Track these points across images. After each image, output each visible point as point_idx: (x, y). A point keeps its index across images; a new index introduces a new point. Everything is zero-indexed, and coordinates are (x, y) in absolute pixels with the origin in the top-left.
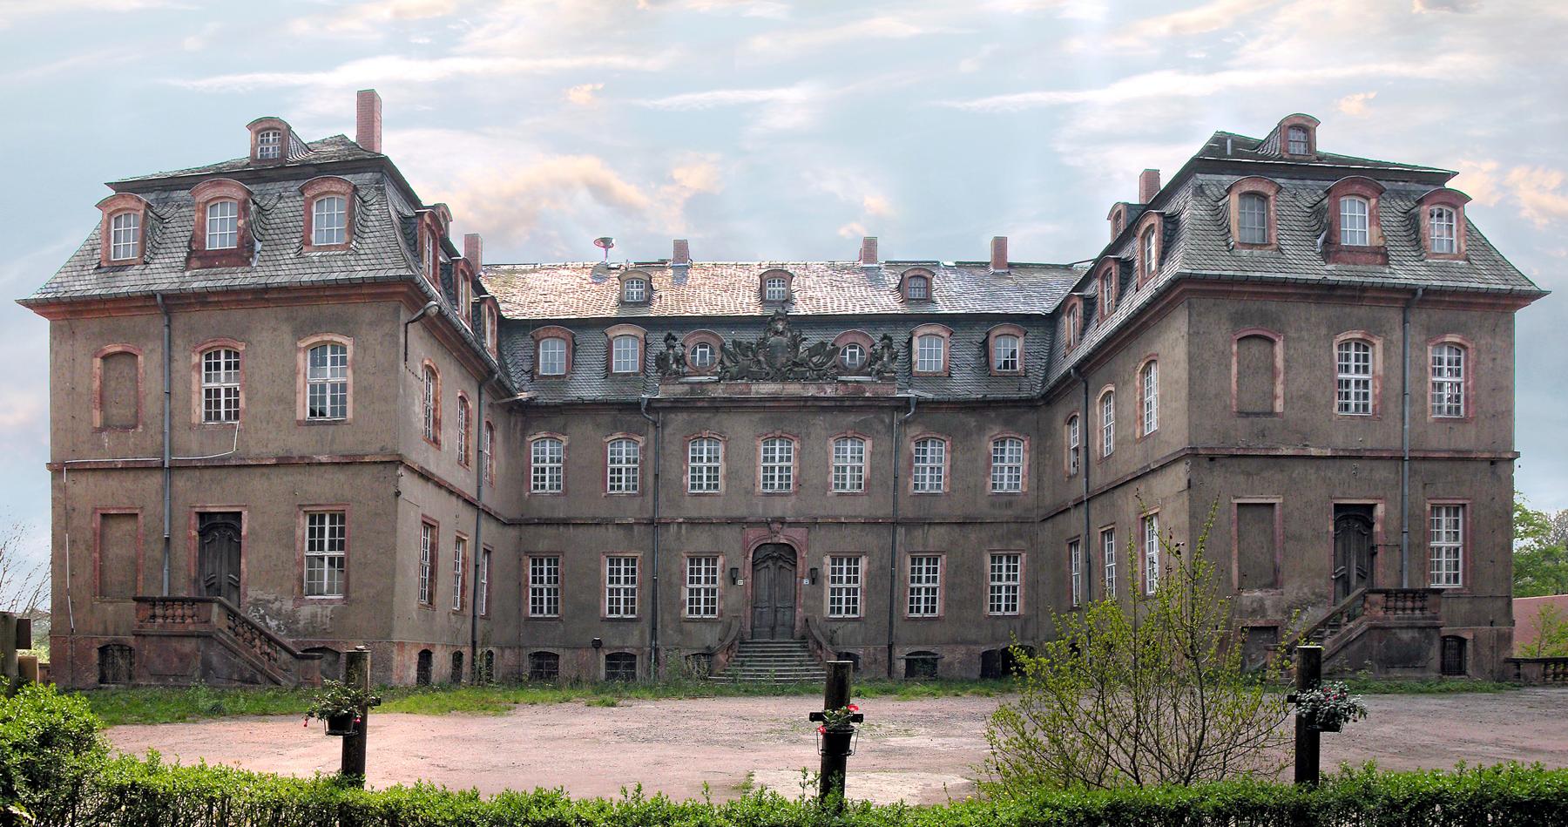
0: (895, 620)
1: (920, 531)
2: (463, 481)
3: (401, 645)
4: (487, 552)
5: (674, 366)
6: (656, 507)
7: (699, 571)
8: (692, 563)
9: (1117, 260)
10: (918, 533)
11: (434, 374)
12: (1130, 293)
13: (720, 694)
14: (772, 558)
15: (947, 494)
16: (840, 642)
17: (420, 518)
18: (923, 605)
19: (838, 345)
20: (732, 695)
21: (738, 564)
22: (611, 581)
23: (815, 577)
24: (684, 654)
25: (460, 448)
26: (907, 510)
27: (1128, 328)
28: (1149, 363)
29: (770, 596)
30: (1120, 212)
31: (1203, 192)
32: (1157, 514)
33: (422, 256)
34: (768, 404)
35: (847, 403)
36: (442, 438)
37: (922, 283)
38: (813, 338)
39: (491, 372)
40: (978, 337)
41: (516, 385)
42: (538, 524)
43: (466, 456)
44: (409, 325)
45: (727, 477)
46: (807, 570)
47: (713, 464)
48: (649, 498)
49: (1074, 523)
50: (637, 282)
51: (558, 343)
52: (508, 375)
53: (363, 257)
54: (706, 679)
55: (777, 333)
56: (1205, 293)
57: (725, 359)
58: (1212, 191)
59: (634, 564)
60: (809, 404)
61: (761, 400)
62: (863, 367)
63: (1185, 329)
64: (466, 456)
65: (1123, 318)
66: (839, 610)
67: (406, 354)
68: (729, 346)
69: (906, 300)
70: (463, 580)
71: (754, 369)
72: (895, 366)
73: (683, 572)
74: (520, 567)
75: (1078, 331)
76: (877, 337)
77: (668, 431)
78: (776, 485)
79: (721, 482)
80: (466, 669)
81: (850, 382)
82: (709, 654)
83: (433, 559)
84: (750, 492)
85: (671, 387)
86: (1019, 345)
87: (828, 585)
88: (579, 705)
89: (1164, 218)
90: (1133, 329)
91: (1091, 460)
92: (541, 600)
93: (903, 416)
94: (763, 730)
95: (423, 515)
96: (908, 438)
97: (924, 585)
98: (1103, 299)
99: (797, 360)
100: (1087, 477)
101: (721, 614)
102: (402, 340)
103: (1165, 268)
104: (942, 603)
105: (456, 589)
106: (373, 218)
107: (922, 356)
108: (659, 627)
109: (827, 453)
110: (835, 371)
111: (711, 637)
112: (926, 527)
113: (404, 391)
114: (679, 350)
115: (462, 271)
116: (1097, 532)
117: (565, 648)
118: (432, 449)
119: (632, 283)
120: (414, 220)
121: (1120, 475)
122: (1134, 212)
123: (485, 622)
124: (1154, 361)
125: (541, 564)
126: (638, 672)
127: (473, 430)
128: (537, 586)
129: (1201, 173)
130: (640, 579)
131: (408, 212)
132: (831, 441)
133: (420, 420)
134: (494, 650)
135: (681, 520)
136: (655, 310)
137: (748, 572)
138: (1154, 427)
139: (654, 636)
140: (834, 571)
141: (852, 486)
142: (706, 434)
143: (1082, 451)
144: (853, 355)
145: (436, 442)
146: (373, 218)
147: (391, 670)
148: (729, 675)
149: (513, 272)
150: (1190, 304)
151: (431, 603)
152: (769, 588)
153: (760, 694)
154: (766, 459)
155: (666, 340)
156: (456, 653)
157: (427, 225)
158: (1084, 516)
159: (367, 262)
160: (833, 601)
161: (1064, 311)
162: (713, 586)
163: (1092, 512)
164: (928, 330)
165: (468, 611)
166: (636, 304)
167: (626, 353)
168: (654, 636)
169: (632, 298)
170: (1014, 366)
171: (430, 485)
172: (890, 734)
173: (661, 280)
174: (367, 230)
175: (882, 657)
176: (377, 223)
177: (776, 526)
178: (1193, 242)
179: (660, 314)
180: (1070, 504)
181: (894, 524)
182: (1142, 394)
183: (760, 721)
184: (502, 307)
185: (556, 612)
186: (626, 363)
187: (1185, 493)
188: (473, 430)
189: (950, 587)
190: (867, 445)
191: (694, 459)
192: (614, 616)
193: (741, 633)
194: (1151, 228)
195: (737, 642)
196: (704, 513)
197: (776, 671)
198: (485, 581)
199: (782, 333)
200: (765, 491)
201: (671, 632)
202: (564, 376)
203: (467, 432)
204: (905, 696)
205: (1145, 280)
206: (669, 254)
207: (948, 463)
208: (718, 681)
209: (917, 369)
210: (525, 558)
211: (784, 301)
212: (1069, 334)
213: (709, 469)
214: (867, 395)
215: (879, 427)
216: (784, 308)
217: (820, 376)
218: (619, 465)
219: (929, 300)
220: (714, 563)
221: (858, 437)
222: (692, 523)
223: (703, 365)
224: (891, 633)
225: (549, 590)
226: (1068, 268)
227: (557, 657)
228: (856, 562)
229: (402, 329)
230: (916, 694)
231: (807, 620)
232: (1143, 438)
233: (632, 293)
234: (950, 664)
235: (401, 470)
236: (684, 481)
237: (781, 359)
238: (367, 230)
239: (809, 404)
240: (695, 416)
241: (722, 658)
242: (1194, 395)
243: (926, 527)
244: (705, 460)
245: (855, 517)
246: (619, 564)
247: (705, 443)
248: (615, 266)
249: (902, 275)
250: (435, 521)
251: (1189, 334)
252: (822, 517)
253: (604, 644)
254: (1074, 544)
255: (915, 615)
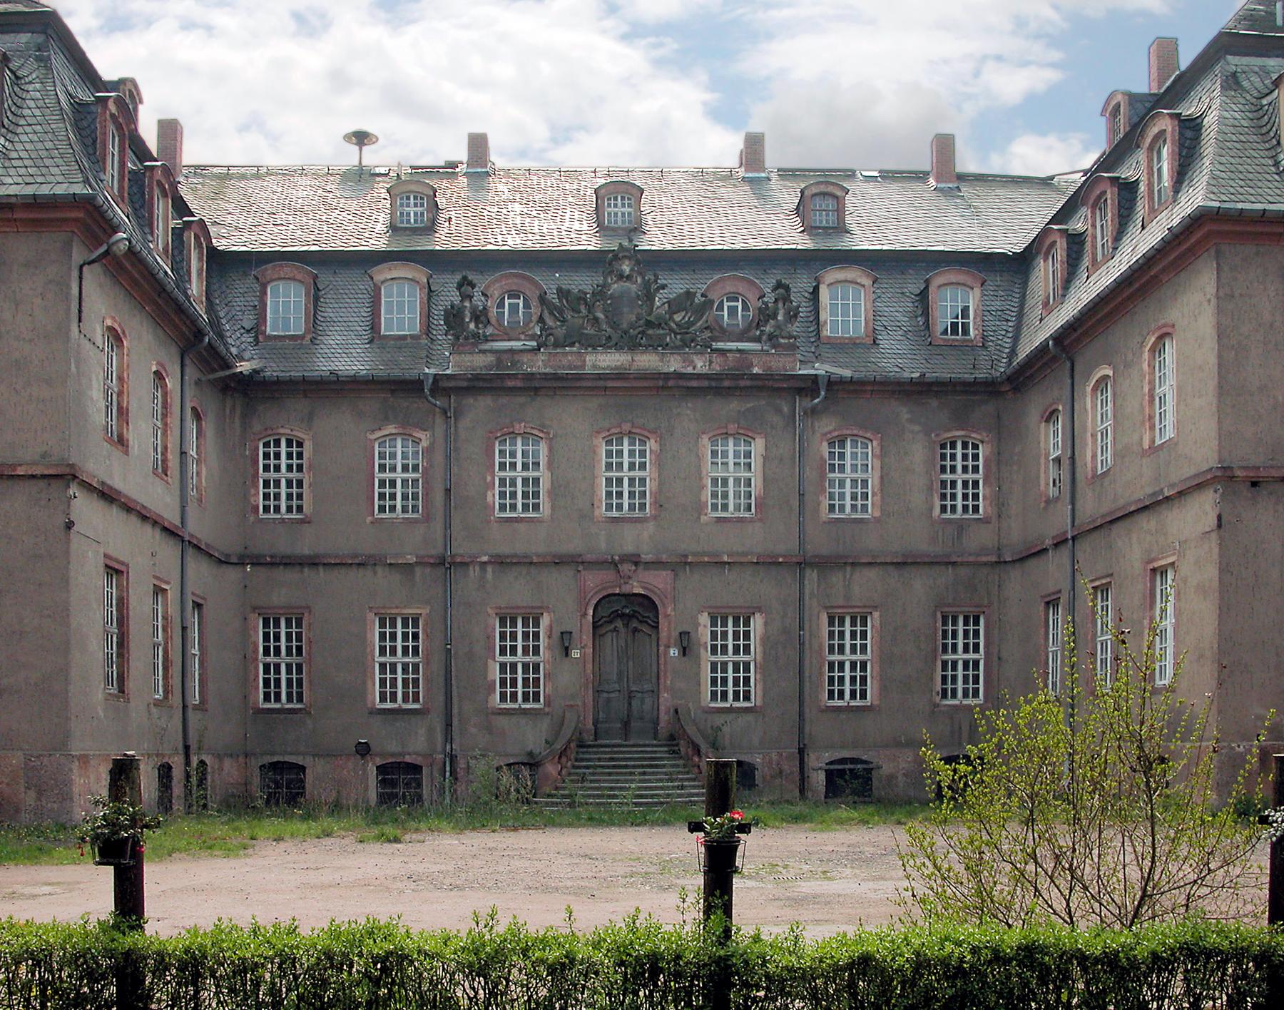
0: (807, 710)
1: (840, 575)
2: (161, 500)
3: (84, 759)
4: (198, 606)
5: (472, 326)
6: (448, 539)
7: (514, 637)
8: (503, 623)
9: (1114, 180)
10: (837, 579)
11: (119, 340)
12: (1134, 229)
13: (550, 823)
14: (622, 616)
15: (877, 520)
16: (727, 743)
17: (101, 561)
18: (847, 688)
19: (710, 296)
20: (570, 825)
21: (572, 625)
22: (382, 651)
23: (686, 644)
24: (495, 763)
25: (156, 450)
26: (820, 544)
27: (1131, 284)
28: (1161, 338)
29: (620, 674)
30: (1118, 105)
31: (1238, 83)
32: (1173, 564)
33: (104, 163)
34: (610, 384)
35: (726, 383)
36: (131, 436)
37: (831, 204)
38: (676, 285)
39: (199, 334)
40: (915, 287)
41: (234, 351)
42: (272, 564)
43: (164, 461)
44: (85, 269)
45: (553, 493)
46: (675, 634)
47: (531, 474)
48: (438, 527)
49: (1053, 570)
50: (415, 198)
51: (293, 286)
52: (221, 336)
53: (15, 163)
54: (528, 802)
55: (621, 277)
56: (1242, 237)
57: (546, 316)
58: (1252, 83)
59: (416, 625)
60: (671, 383)
61: (600, 377)
62: (748, 329)
63: (1211, 289)
64: (164, 461)
65: (1124, 268)
66: (724, 695)
67: (80, 311)
68: (552, 296)
69: (809, 229)
70: (166, 652)
71: (589, 330)
72: (795, 328)
73: (490, 638)
74: (245, 632)
75: (1059, 283)
76: (767, 284)
77: (465, 422)
78: (626, 506)
79: (544, 500)
80: (178, 789)
81: (730, 351)
82: (533, 764)
83: (122, 622)
84: (586, 516)
85: (467, 358)
86: (973, 300)
87: (707, 658)
88: (346, 841)
89: (1181, 121)
90: (1137, 285)
91: (1078, 475)
92: (278, 681)
93: (808, 403)
94: (622, 873)
95: (106, 556)
96: (818, 435)
97: (848, 657)
98: (1095, 237)
99: (651, 318)
100: (1073, 503)
101: (548, 703)
102: (75, 291)
103: (1183, 198)
104: (876, 685)
105: (155, 666)
106: (32, 104)
107: (834, 313)
108: (455, 722)
109: (699, 458)
110: (708, 334)
111: (533, 738)
112: (849, 569)
113: (77, 367)
114: (478, 300)
115: (159, 183)
116: (1085, 584)
117: (314, 756)
118: (117, 453)
119: (408, 198)
120: (93, 108)
121: (1121, 502)
122: (1139, 105)
123: (199, 715)
124: (1168, 334)
125: (277, 625)
126: (425, 792)
127: (174, 421)
128: (271, 659)
129: (1235, 54)
130: (426, 649)
131: (84, 95)
132: (705, 440)
133: (99, 411)
134: (208, 761)
135: (485, 559)
136: (443, 241)
137: (587, 638)
138: (1170, 433)
139: (448, 737)
140: (714, 636)
141: (738, 508)
142: (520, 427)
143: (1066, 463)
144: (733, 311)
145: (122, 442)
146: (32, 104)
147: (71, 799)
148: (564, 796)
149: (227, 176)
150: (1218, 252)
151: (122, 691)
152: (619, 663)
153: (611, 823)
154: (609, 467)
155: (459, 287)
156: (162, 766)
157: (112, 115)
158: (1066, 561)
159: (22, 171)
160: (714, 681)
161: (1038, 253)
162: (535, 659)
163: (1080, 555)
164: (840, 275)
165: (176, 699)
166: (415, 231)
167: (401, 305)
168: (448, 737)
169: (409, 221)
170: (966, 331)
171: (115, 510)
172: (801, 876)
173: (449, 194)
174: (22, 122)
175: (791, 767)
176: (37, 112)
177: (626, 568)
178: (1223, 160)
179: (451, 247)
180: (1048, 542)
181: (802, 565)
182: (1152, 383)
183: (614, 860)
184: (213, 230)
185: (300, 700)
186: (401, 321)
187: (1214, 536)
188: (174, 421)
189: (886, 659)
190: (758, 446)
191: (502, 466)
192: (389, 705)
193: (579, 732)
194: (1163, 132)
195: (573, 745)
196: (520, 548)
197: (639, 788)
198: (196, 651)
199: (629, 278)
200: (609, 514)
201: (473, 730)
202: (302, 337)
203: (166, 424)
204: (825, 825)
205: (1153, 213)
206: (461, 154)
207: (877, 474)
208: (547, 804)
209: (827, 332)
210: (252, 615)
211: (631, 231)
212: (1047, 285)
213: (525, 481)
214: (756, 370)
215: (776, 419)
216: (631, 241)
217: (687, 341)
218: (392, 475)
219: (841, 229)
220: (537, 625)
221: (745, 434)
222: (502, 563)
223: (514, 324)
224: (801, 730)
225: (289, 667)
226: (1046, 182)
227: (302, 769)
228: (747, 623)
229: (75, 274)
230: (840, 822)
231: (676, 711)
232: (1154, 449)
233: (409, 214)
234: (891, 778)
235: (73, 489)
236: (489, 499)
237: (629, 317)
238: (22, 122)
239: (671, 383)
240: (504, 400)
241: (551, 769)
242: (1224, 389)
243: (849, 569)
244: (519, 466)
245: (745, 554)
246: (393, 625)
247: (519, 442)
248: (383, 171)
249: (802, 192)
250: (122, 563)
251: (1218, 298)
252: (694, 554)
253: (374, 749)
254: (1051, 603)
255: (837, 703)
